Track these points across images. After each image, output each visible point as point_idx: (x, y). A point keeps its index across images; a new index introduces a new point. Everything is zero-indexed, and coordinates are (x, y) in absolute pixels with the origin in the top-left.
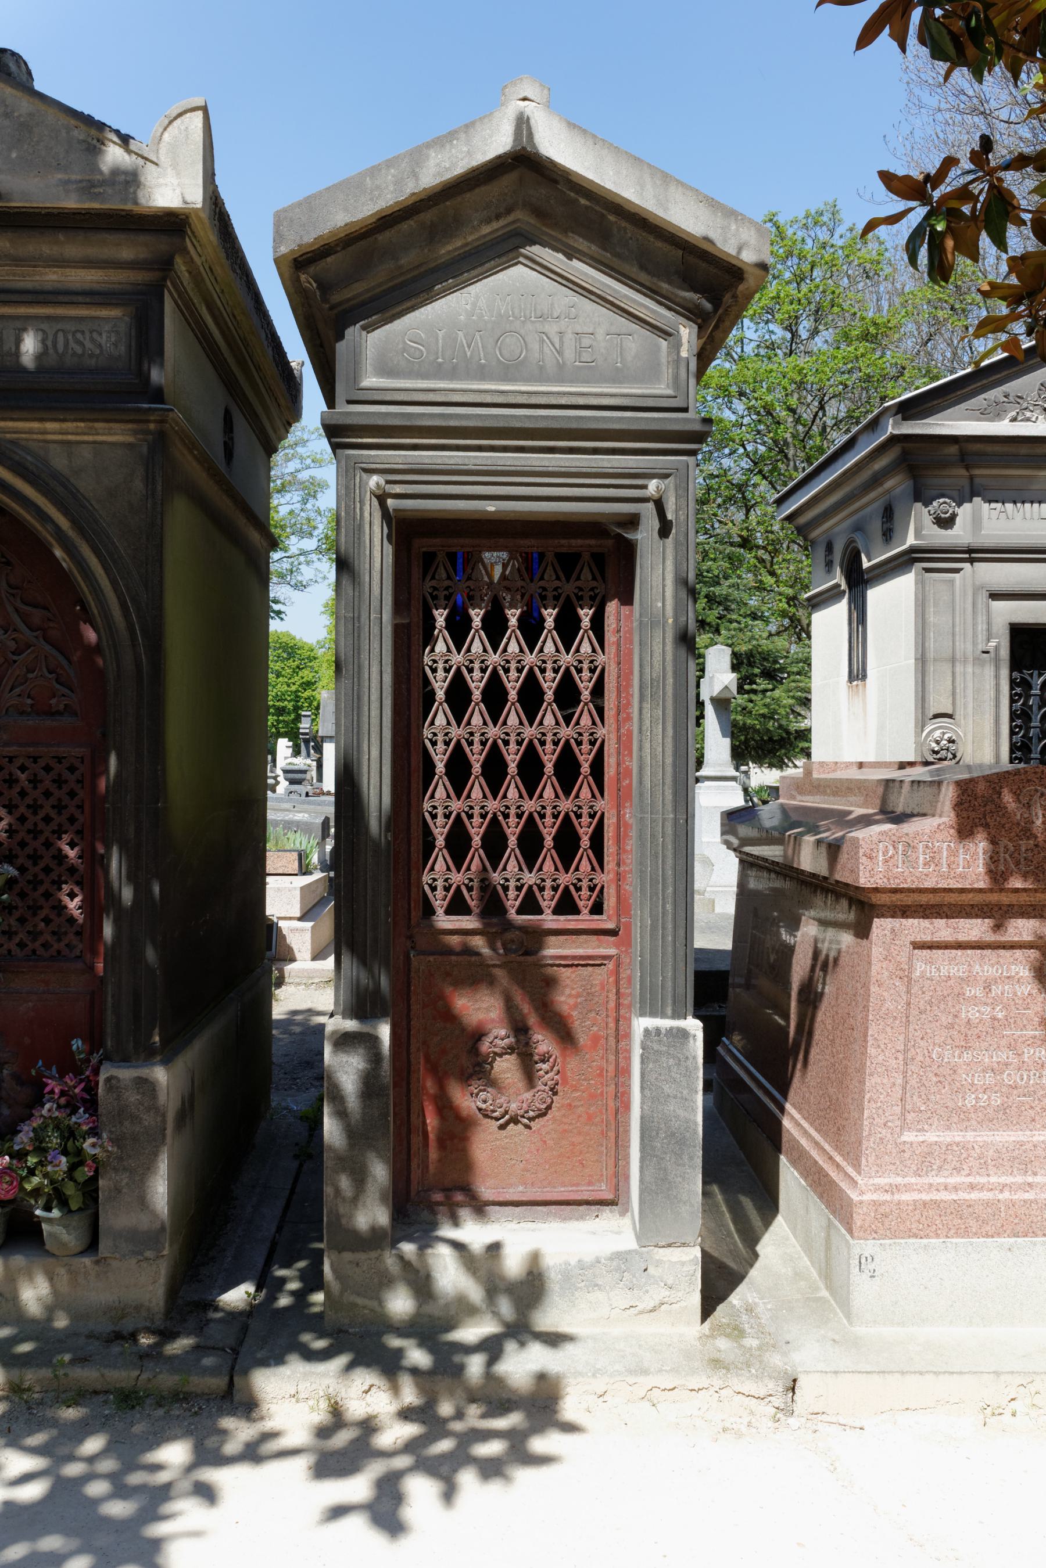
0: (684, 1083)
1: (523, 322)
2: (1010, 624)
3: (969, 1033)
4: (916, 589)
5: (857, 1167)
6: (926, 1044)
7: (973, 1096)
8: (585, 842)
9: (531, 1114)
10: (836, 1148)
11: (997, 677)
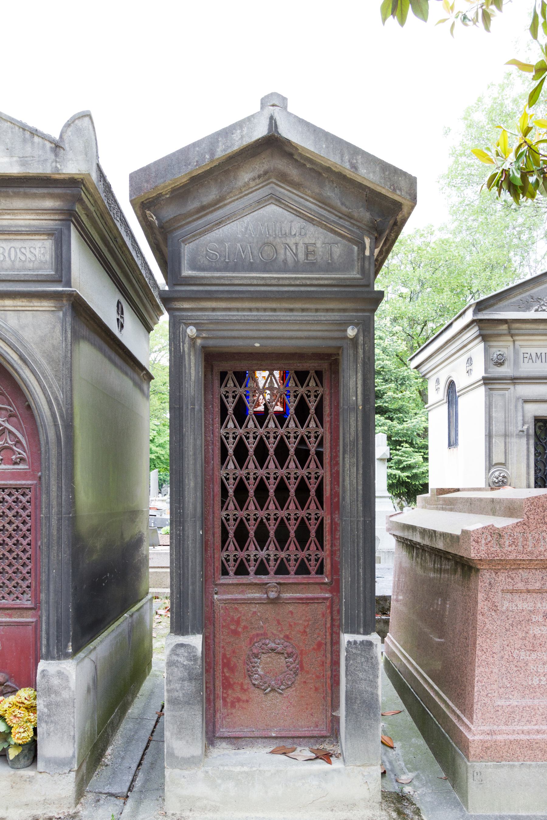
0: (371, 672)
1: (275, 238)
2: (535, 417)
3: (535, 642)
4: (486, 399)
5: (471, 719)
6: (510, 649)
7: (538, 679)
8: (313, 534)
9: (282, 687)
10: (456, 705)
11: (528, 444)
